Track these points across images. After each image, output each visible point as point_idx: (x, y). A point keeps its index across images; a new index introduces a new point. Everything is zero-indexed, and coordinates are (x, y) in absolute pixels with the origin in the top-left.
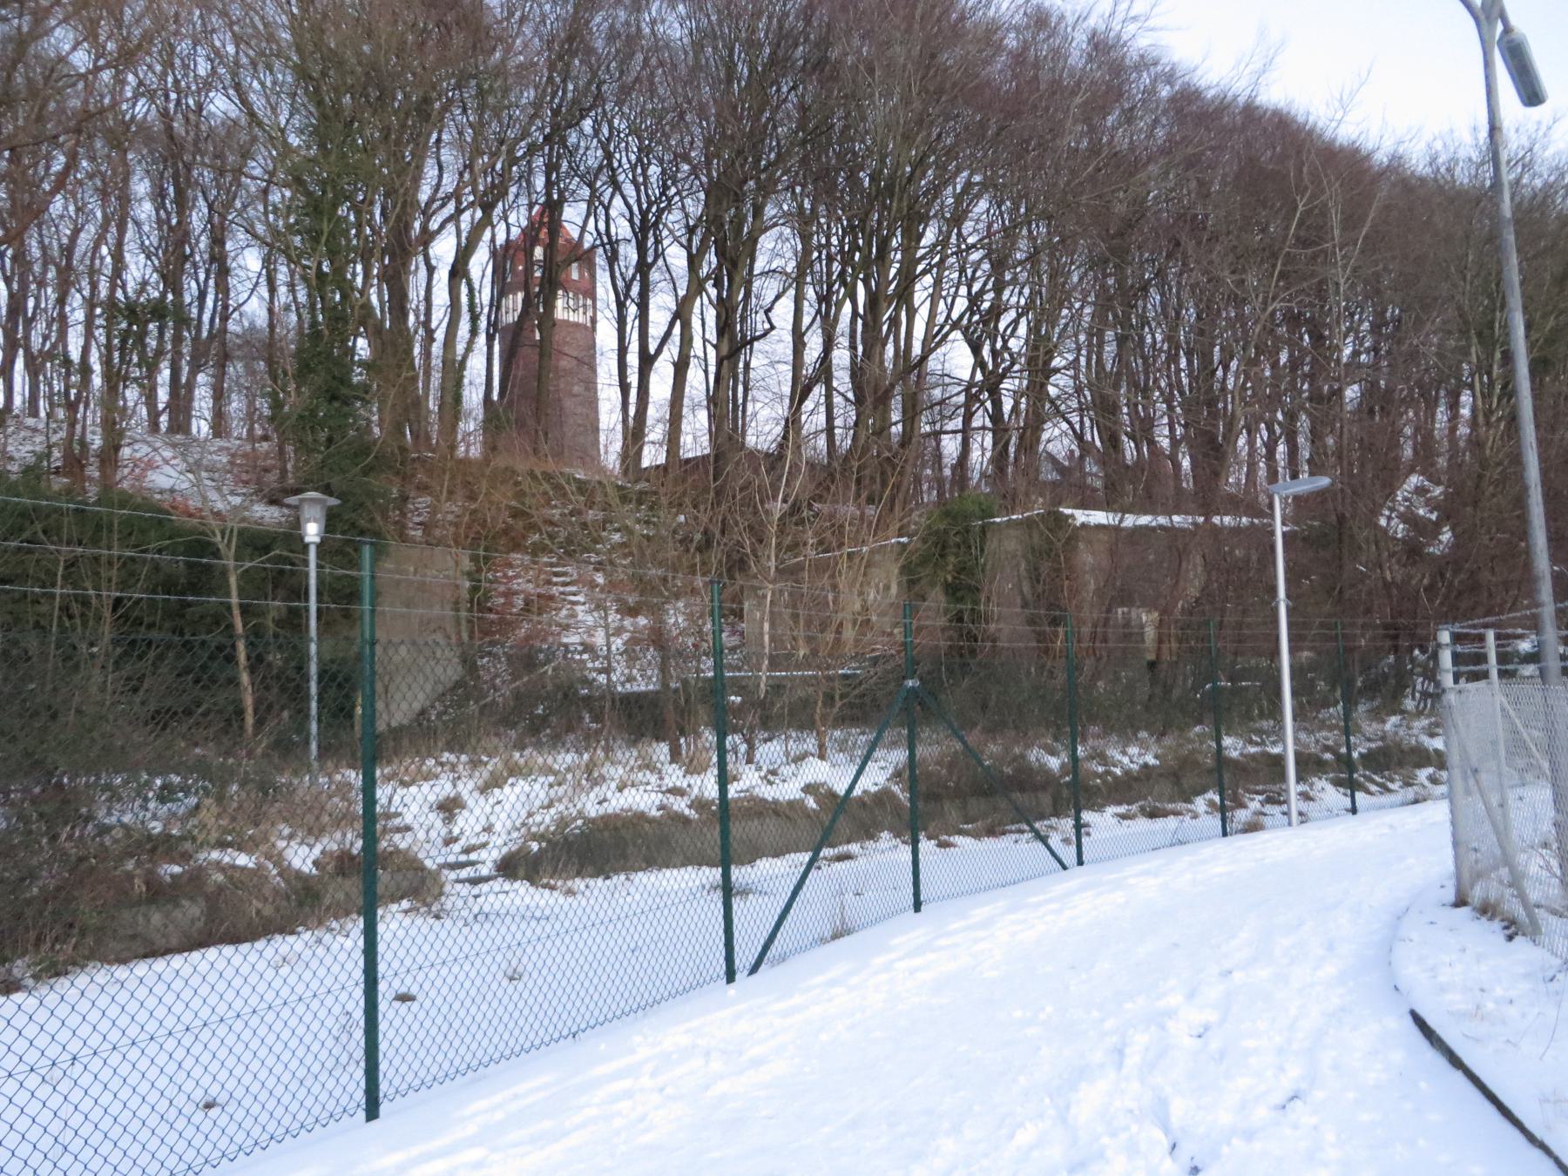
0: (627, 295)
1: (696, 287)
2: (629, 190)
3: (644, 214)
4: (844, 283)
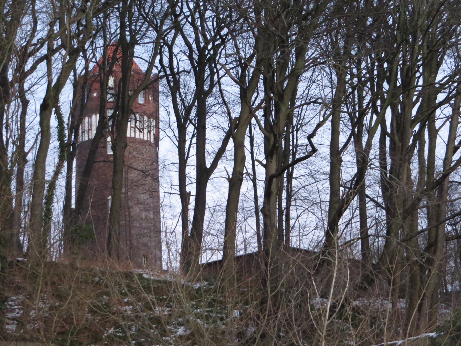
0: (187, 118)
1: (248, 111)
2: (188, 29)
3: (201, 51)
4: (375, 110)
